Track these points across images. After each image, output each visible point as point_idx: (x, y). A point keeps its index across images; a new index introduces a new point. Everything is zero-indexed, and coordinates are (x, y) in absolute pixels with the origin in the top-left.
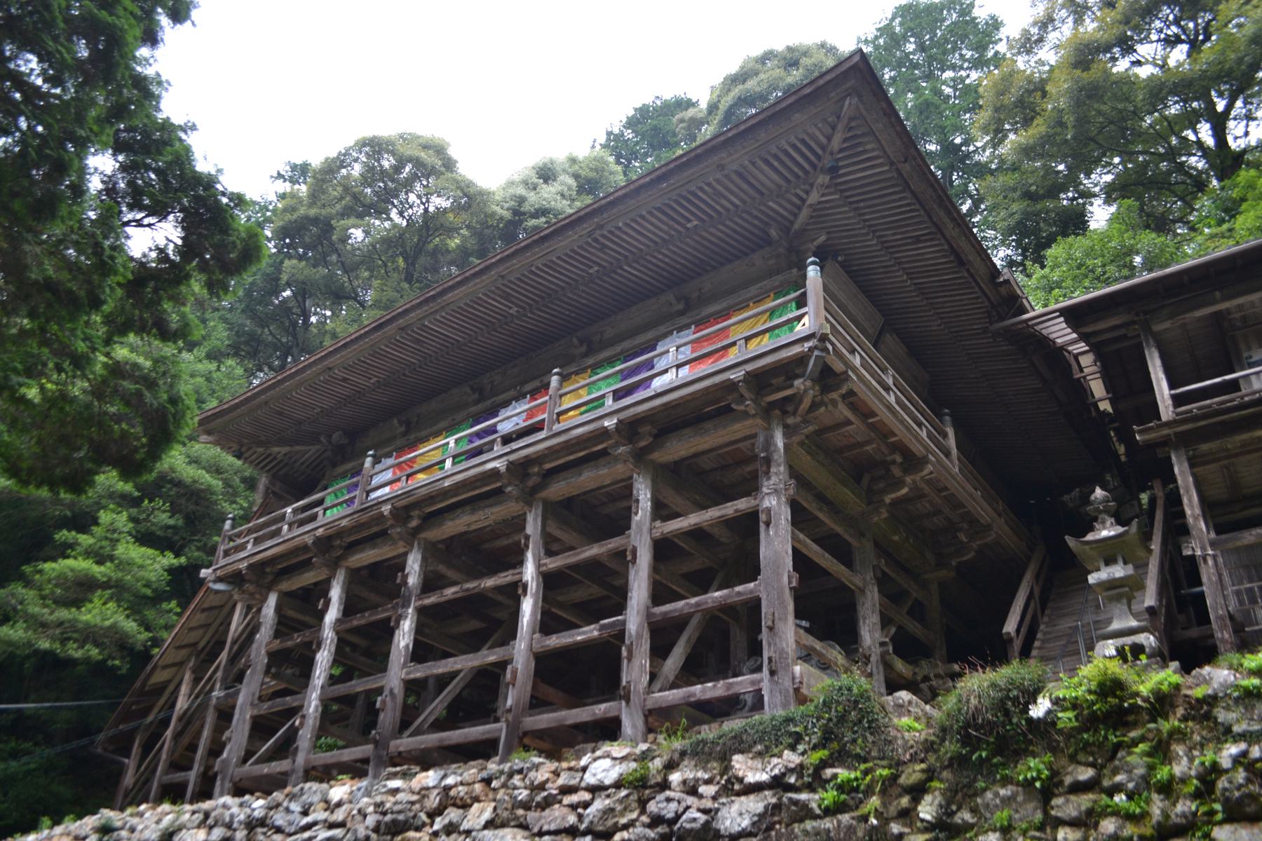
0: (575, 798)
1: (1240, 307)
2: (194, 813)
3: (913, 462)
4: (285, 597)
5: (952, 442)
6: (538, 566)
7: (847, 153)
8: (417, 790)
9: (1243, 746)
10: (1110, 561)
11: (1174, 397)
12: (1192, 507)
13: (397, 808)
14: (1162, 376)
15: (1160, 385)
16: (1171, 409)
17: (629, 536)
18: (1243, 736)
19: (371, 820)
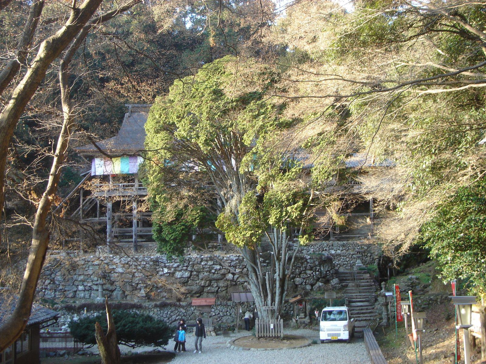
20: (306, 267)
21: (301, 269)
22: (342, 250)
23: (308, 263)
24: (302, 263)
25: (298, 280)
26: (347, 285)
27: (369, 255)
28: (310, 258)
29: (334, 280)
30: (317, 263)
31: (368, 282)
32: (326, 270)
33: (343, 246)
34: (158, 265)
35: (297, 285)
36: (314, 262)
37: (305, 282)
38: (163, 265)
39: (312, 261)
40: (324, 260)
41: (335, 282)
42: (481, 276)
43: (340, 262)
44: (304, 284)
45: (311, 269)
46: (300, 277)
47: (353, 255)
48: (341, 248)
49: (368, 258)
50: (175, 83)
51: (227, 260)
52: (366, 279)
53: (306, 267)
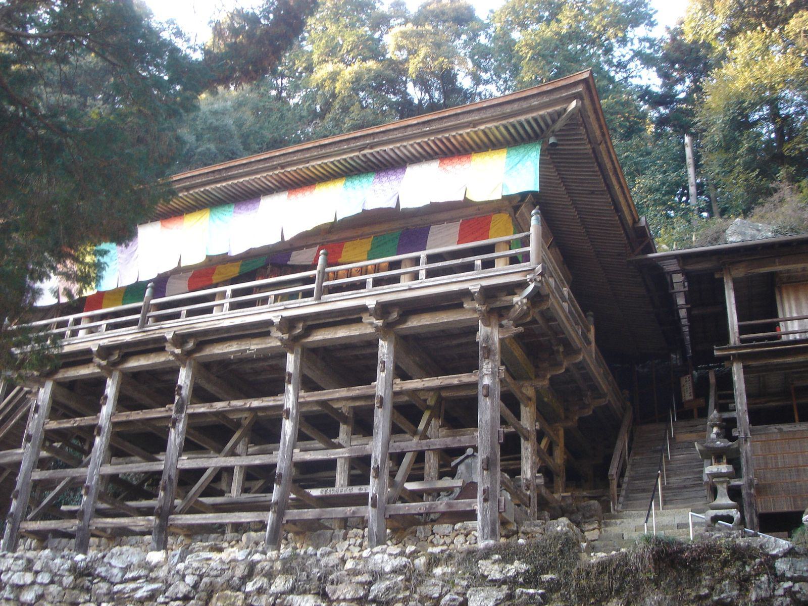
0: (360, 578)
1: (788, 271)
2: (17, 559)
3: (570, 350)
4: (59, 384)
5: (592, 335)
6: (297, 397)
7: (546, 99)
8: (227, 561)
9: (790, 584)
10: (718, 460)
11: (740, 327)
12: (741, 404)
13: (212, 573)
14: (734, 311)
15: (732, 317)
16: (737, 335)
17: (375, 386)
18: (791, 579)
19: (190, 580)
23: (782, 578)
24: (744, 583)
28: (790, 553)
34: (88, 590)
38: (103, 587)
42: (13, 440)
50: (270, 136)
51: (355, 572)
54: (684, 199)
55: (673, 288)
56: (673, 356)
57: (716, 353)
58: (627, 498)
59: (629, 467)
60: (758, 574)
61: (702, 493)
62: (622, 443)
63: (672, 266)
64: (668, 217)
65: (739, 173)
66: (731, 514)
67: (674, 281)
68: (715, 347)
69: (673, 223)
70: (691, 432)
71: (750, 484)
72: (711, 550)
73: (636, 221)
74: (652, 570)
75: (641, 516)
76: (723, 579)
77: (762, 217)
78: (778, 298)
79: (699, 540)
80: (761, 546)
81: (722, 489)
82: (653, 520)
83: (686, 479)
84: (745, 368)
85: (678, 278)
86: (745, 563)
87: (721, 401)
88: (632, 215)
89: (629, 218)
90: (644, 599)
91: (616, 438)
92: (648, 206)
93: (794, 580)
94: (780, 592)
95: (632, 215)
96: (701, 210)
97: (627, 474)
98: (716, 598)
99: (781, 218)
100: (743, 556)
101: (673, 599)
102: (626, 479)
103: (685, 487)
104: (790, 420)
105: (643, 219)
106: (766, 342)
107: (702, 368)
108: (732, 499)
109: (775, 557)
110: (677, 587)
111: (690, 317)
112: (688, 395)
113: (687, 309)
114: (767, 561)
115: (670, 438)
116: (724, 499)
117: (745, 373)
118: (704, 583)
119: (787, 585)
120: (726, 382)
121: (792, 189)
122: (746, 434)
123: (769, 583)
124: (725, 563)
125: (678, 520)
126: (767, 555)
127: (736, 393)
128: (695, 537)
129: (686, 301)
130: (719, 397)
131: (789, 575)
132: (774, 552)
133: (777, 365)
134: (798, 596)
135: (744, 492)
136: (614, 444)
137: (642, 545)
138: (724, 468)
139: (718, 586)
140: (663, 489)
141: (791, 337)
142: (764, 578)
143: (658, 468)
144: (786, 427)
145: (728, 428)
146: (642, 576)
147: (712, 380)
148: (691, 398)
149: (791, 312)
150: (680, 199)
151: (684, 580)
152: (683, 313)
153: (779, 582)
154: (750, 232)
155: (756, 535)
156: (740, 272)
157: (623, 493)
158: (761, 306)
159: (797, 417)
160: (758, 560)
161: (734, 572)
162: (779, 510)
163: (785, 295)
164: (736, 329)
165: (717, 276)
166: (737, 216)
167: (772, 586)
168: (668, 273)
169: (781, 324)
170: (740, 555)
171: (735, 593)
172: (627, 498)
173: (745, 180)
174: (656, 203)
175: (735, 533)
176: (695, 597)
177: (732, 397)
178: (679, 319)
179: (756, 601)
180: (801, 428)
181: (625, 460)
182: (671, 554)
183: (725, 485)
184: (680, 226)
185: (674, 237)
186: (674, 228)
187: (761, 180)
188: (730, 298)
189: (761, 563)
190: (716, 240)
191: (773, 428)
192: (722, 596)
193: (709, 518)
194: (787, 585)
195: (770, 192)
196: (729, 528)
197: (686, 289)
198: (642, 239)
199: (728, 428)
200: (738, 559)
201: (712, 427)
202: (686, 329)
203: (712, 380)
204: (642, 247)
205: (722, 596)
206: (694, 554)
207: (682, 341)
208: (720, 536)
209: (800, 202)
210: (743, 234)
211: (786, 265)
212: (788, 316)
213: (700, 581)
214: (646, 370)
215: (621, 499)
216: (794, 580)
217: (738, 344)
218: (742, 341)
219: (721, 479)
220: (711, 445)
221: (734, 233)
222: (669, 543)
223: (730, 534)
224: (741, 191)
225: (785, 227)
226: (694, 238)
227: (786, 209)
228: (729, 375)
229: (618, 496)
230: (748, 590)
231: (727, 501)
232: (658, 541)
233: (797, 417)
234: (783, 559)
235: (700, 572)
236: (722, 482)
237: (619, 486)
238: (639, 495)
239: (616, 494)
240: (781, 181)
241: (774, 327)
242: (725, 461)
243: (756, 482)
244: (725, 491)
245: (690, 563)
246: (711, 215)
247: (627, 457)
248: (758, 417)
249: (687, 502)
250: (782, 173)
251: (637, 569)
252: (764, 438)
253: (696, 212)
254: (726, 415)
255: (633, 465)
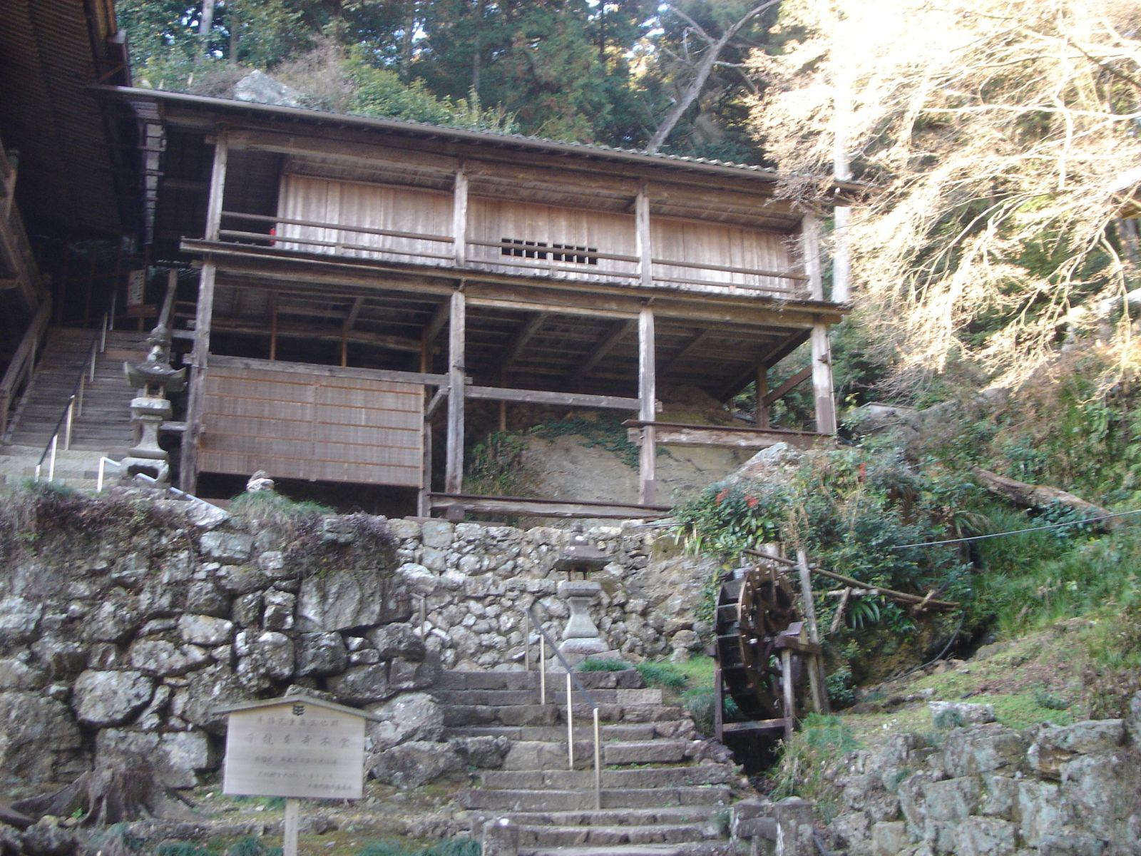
1: (304, 158)
9: (215, 565)
10: (153, 391)
12: (203, 323)
15: (215, 201)
16: (217, 227)
20: (179, 589)
21: (145, 599)
22: (475, 573)
23: (205, 557)
24: (156, 559)
25: (105, 690)
26: (503, 753)
27: (636, 604)
28: (223, 526)
29: (399, 704)
30: (273, 561)
31: (656, 734)
32: (345, 621)
33: (485, 547)
35: (89, 731)
36: (253, 552)
37: (165, 710)
39: (237, 545)
40: (334, 546)
41: (412, 722)
43: (458, 632)
44: (149, 720)
45: (224, 603)
46: (123, 666)
47: (540, 595)
48: (470, 561)
49: (633, 624)
52: (643, 719)
53: (179, 589)
54: (195, 23)
55: (145, 143)
56: (126, 239)
57: (183, 247)
58: (21, 426)
59: (31, 383)
60: (175, 550)
61: (127, 435)
62: (28, 347)
63: (148, 112)
64: (164, 41)
65: (276, 8)
66: (156, 466)
67: (149, 133)
68: (183, 238)
69: (168, 53)
70: (129, 349)
71: (194, 432)
72: (119, 511)
73: (111, 34)
74: (33, 529)
75: (35, 455)
76: (128, 552)
77: (290, 78)
78: (282, 190)
79: (106, 495)
80: (187, 513)
81: (151, 431)
82: (52, 462)
83: (108, 413)
84: (218, 274)
85: (155, 131)
86: (161, 533)
87: (179, 314)
88: (108, 24)
89: (102, 26)
90: (16, 567)
91: (20, 340)
92: (139, 19)
93: (223, 561)
94: (202, 575)
95: (108, 24)
96: (212, 47)
97: (27, 393)
98: (115, 575)
99: (314, 86)
100: (161, 524)
101: (57, 571)
102: (24, 400)
103: (105, 423)
104: (262, 354)
105: (122, 33)
106: (253, 245)
107: (161, 265)
108: (161, 446)
109: (203, 529)
110: (64, 556)
111: (160, 189)
112: (136, 297)
113: (159, 177)
114: (191, 534)
115: (98, 353)
116: (150, 445)
117: (217, 281)
118: (102, 554)
119: (212, 566)
120: (189, 289)
121: (338, 50)
122: (201, 364)
123: (190, 562)
124: (136, 530)
125: (86, 466)
126: (193, 525)
127: (200, 306)
128: (103, 489)
129: (160, 166)
130: (178, 308)
131: (216, 554)
132: (202, 523)
133: (262, 279)
134: (224, 582)
135: (184, 441)
136: (16, 348)
137: (23, 493)
138: (158, 403)
139: (121, 560)
140: (74, 421)
141: (287, 246)
142: (184, 555)
143: (71, 390)
144: (255, 364)
145: (178, 350)
146: (17, 536)
147: (173, 282)
148: (140, 302)
149: (294, 213)
150: (189, 22)
151: (76, 548)
152: (151, 182)
153: (202, 561)
154: (269, 93)
155: (183, 498)
156: (240, 143)
157: (16, 419)
158: (257, 195)
159: (273, 353)
160: (179, 531)
161: (145, 543)
162: (226, 471)
163: (292, 189)
164: (217, 220)
165: (208, 141)
166: (259, 66)
167: (192, 565)
168: (142, 120)
169: (279, 226)
170: (157, 521)
171: (142, 571)
172: (21, 426)
173: (282, 21)
174: (152, 17)
175: (157, 492)
176: (88, 571)
177: (193, 311)
178: (144, 190)
179: (168, 584)
180: (274, 368)
181: (27, 374)
182: (63, 510)
183: (155, 427)
184: (176, 59)
185: (164, 73)
186: (167, 60)
187: (302, 27)
188: (218, 175)
189: (183, 536)
190: (222, 91)
191: (239, 362)
192: (125, 573)
193: (125, 468)
194: (212, 566)
195: (309, 47)
196: (150, 484)
197: (163, 149)
198: (115, 63)
199: (178, 350)
200: (155, 527)
201: (154, 344)
202: (151, 205)
203: (173, 282)
204: (111, 73)
205: (125, 573)
206: (96, 513)
207: (143, 221)
208: (134, 494)
209: (344, 70)
210: (259, 93)
211: (304, 148)
212: (290, 217)
213: (98, 550)
214: (84, 251)
215: (12, 427)
216: (223, 561)
217: (215, 240)
218: (222, 237)
219: (152, 418)
220: (146, 369)
221: (246, 89)
222: (63, 495)
223: (150, 493)
224: (270, 34)
225: (315, 99)
226: (190, 81)
227: (323, 75)
228: (197, 280)
229: (9, 422)
230: (159, 569)
231: (154, 448)
232: (48, 490)
233: (273, 353)
234: (213, 533)
235: (99, 539)
236: (153, 422)
237: (12, 408)
238: (38, 425)
239: (5, 420)
240: (327, 36)
241: (268, 227)
242: (161, 393)
243: (202, 429)
244: (154, 434)
245: (89, 525)
246: (226, 56)
247: (31, 369)
248: (222, 344)
249: (104, 444)
250: (332, 26)
251: (11, 526)
252: (225, 373)
253: (204, 46)
254: (181, 334)
255: (38, 382)
